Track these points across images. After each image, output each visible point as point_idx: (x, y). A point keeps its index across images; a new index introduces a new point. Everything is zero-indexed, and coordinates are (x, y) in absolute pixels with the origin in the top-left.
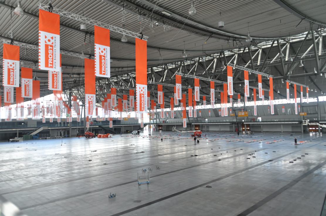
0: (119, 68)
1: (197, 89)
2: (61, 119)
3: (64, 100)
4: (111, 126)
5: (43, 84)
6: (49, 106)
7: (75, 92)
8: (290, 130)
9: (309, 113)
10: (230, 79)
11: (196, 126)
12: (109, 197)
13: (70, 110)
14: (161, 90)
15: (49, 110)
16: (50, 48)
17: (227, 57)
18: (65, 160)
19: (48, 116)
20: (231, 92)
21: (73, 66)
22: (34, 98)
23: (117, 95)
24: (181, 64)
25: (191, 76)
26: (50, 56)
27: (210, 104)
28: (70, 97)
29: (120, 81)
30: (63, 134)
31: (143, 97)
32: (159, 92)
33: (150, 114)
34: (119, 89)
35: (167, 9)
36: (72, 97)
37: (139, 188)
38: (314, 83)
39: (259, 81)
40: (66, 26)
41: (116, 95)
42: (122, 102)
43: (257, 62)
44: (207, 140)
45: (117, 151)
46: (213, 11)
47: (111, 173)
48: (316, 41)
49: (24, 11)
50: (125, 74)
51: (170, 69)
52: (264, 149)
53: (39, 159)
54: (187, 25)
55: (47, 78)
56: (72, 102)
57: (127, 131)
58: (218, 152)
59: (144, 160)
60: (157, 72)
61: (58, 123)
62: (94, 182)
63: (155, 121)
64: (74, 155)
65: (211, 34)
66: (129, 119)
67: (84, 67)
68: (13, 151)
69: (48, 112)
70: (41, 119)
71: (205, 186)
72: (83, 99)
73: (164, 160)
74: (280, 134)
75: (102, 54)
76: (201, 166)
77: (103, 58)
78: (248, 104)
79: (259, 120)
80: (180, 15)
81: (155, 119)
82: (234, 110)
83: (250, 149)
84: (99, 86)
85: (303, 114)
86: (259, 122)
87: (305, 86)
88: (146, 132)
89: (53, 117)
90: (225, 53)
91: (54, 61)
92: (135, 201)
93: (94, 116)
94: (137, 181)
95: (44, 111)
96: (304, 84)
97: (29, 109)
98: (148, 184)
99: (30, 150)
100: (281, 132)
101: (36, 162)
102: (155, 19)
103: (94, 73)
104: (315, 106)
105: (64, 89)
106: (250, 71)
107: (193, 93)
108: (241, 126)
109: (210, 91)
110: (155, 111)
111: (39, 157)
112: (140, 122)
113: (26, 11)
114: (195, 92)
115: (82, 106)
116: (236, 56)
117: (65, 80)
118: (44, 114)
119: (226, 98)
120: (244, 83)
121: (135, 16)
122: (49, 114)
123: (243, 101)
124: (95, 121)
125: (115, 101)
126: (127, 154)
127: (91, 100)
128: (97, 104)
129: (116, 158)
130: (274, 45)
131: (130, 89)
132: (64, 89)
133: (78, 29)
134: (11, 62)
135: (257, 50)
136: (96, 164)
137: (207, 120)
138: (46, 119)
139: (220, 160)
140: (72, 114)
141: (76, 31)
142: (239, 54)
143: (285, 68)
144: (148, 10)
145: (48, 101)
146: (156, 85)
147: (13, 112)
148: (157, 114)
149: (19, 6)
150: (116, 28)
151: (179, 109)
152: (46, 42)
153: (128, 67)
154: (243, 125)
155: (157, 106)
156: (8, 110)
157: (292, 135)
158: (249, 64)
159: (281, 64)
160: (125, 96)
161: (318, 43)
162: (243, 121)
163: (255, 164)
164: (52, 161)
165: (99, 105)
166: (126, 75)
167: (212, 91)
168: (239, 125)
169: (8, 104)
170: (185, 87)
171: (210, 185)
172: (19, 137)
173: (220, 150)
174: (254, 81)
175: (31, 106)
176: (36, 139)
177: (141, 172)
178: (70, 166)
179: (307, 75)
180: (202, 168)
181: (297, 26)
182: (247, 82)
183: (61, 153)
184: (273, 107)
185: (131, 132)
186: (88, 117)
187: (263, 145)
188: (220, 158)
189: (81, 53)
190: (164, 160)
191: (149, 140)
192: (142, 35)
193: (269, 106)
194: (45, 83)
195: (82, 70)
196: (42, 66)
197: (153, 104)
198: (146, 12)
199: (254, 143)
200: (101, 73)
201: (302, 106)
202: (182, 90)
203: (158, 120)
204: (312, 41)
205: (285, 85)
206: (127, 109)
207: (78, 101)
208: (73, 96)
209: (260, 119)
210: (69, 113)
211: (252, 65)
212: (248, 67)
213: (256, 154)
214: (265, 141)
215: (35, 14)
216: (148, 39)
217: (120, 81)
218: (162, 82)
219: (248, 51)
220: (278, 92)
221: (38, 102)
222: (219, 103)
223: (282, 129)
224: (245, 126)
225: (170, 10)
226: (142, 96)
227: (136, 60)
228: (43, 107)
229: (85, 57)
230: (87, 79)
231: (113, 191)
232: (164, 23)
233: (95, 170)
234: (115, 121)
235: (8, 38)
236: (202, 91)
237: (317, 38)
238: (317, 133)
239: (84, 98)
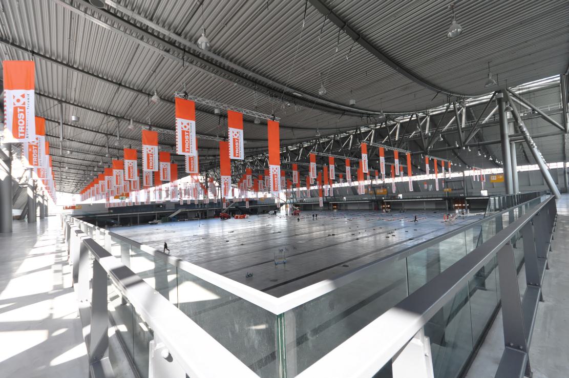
0: (253, 148)
1: (332, 167)
2: (199, 200)
3: (201, 181)
4: (247, 206)
5: (180, 167)
6: (186, 187)
7: (211, 173)
8: (433, 207)
9: (454, 188)
10: (365, 156)
11: (334, 205)
12: (247, 277)
13: (207, 192)
14: (294, 170)
15: (187, 192)
16: (186, 133)
17: (363, 133)
18: (203, 241)
19: (185, 198)
20: (365, 169)
21: (209, 148)
22: (172, 181)
23: (253, 176)
24: (316, 142)
25: (326, 155)
26: (21, 122)
27: (347, 182)
28: (206, 178)
29: (255, 161)
30: (200, 216)
31: (277, 177)
32: (294, 172)
33: (286, 194)
34: (253, 170)
35: (298, 90)
36: (208, 179)
37: (276, 268)
38: (458, 157)
39: (395, 157)
40: (202, 111)
41: (251, 176)
42: (258, 182)
43: (395, 138)
44: (346, 219)
45: (255, 232)
46: (412, 35)
47: (249, 253)
48: (459, 112)
49: (161, 98)
50: (260, 154)
51: (305, 147)
52: (404, 227)
53: (179, 240)
54: (318, 104)
55: (184, 161)
56: (209, 184)
57: (264, 211)
58: (356, 230)
59: (281, 240)
60: (292, 151)
61: (195, 205)
62: (232, 262)
63: (292, 200)
64: (211, 236)
65: (344, 112)
66: (265, 199)
67: (219, 149)
68: (152, 234)
69: (185, 194)
70: (179, 201)
71: (342, 265)
72: (219, 180)
73: (301, 240)
74: (423, 211)
75: (236, 137)
76: (339, 245)
77: (236, 141)
78: (388, 181)
79: (400, 198)
80: (311, 95)
81: (292, 198)
82: (373, 187)
83: (390, 228)
84: (235, 167)
85: (448, 190)
86: (400, 199)
87: (446, 161)
88: (283, 211)
89: (191, 198)
90: (362, 129)
91: (190, 146)
92: (271, 281)
93: (230, 197)
94: (273, 261)
95: (181, 193)
96: (445, 158)
97: (167, 191)
98: (284, 263)
99: (168, 232)
100: (423, 209)
101: (174, 243)
102: (287, 100)
103: (229, 156)
104: (461, 181)
105: (201, 171)
106: (387, 148)
107: (329, 171)
108: (380, 204)
109: (345, 168)
110: (291, 190)
111: (177, 239)
112: (276, 201)
113: (162, 97)
114: (330, 171)
115: (219, 187)
116: (373, 131)
117: (201, 162)
118: (181, 196)
119: (362, 176)
120: (379, 160)
121: (267, 98)
122: (187, 196)
123: (380, 177)
124: (231, 201)
125: (251, 181)
126: (265, 234)
127: (237, 136)
128: (233, 185)
129: (253, 238)
130: (413, 119)
131: (265, 169)
132: (201, 171)
133: (212, 113)
134: (150, 147)
135: (395, 125)
136: (233, 245)
137: (345, 198)
138: (184, 201)
139: (357, 239)
140: (209, 195)
141: (211, 115)
142: (376, 130)
143: (425, 143)
144: (279, 91)
145: (184, 183)
146: (291, 165)
147: (152, 194)
148: (294, 193)
149: (156, 94)
150: (248, 111)
151: (316, 187)
152: (182, 128)
153: (262, 147)
154: (383, 203)
155: (293, 185)
156: (147, 194)
157: (435, 212)
158: (387, 139)
159: (420, 138)
160: (259, 177)
161: (461, 115)
162: (383, 198)
163: (395, 243)
164: (191, 242)
165: (235, 186)
166: (261, 155)
167: (348, 168)
168: (379, 203)
169: (147, 188)
170: (320, 166)
171: (346, 264)
172: (158, 219)
173: (358, 228)
174: (389, 158)
175: (168, 188)
176: (174, 221)
177: (277, 252)
178: (208, 247)
179: (448, 149)
180: (339, 247)
181: (432, 100)
182: (382, 159)
183: (198, 234)
184: (412, 184)
185: (267, 212)
186: (224, 198)
187: (405, 223)
188: (359, 236)
189: (216, 136)
190: (301, 240)
191: (286, 220)
192: (274, 117)
193: (407, 183)
194: (182, 166)
195: (217, 152)
196: (179, 151)
197: (288, 184)
198: (278, 94)
199: (395, 221)
200: (235, 156)
201: (446, 181)
202: (317, 169)
203: (295, 200)
204: (454, 112)
205: (424, 160)
206: (263, 189)
207: (214, 182)
208: (209, 177)
209: (401, 196)
210: (206, 195)
211: (390, 140)
212: (386, 143)
213: (396, 233)
214: (407, 219)
215: (171, 101)
216: (280, 120)
217: (255, 161)
218: (298, 161)
219: (385, 126)
220: (419, 168)
221: (176, 184)
222: (357, 180)
223: (425, 206)
224: (385, 203)
225: (301, 91)
226: (276, 176)
227: (269, 140)
228: (180, 189)
229: (220, 140)
230: (222, 160)
231: (250, 270)
232: (295, 103)
233: (233, 251)
234: (252, 202)
235: (146, 124)
236: (339, 169)
237: (459, 110)
238: (464, 210)
239: (220, 179)
